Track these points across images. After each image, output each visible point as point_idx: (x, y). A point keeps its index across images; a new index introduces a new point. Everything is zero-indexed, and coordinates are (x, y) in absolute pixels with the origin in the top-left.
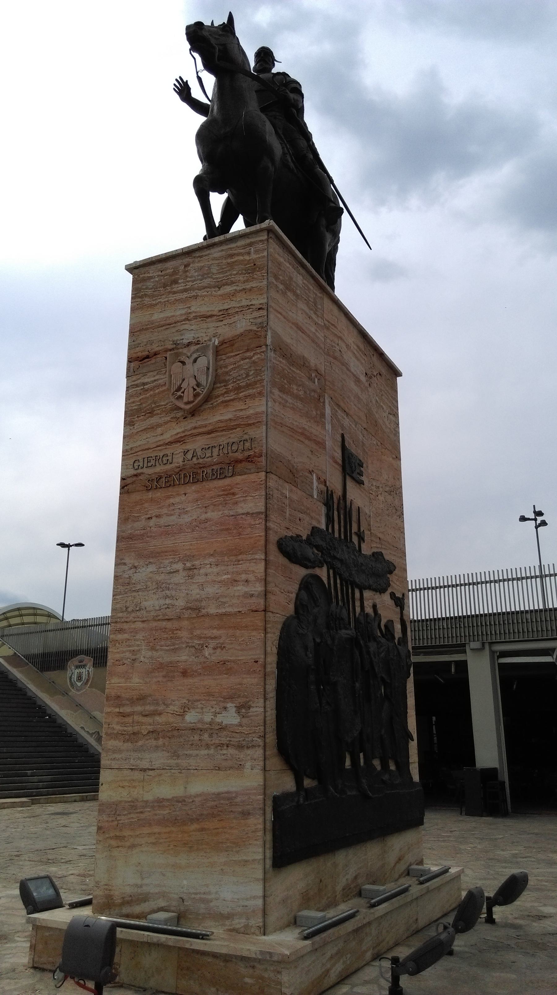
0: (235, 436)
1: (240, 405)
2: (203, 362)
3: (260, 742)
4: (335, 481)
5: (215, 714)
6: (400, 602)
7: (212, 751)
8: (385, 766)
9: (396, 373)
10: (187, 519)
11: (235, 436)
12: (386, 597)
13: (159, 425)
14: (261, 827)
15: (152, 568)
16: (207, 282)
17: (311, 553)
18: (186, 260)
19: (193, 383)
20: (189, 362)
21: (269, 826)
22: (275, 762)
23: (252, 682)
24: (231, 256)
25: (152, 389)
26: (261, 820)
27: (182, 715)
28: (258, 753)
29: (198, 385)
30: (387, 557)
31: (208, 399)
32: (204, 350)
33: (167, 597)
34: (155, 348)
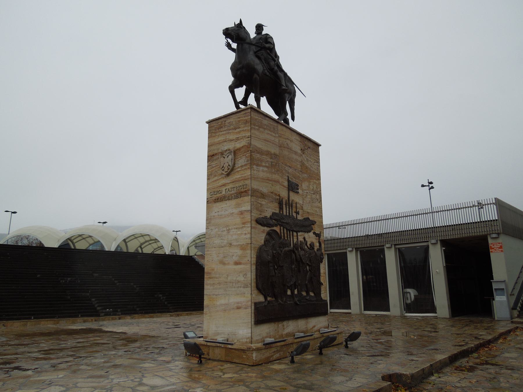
0: (241, 184)
1: (242, 172)
2: (230, 157)
3: (250, 286)
4: (284, 193)
5: (237, 277)
6: (318, 235)
8: (308, 293)
9: (318, 145)
10: (227, 213)
12: (311, 234)
13: (218, 180)
14: (250, 312)
15: (217, 230)
16: (232, 127)
17: (271, 222)
18: (225, 119)
19: (227, 165)
20: (226, 157)
21: (253, 311)
22: (256, 291)
23: (248, 267)
24: (239, 118)
25: (215, 167)
26: (250, 310)
28: (249, 289)
29: (229, 165)
30: (311, 219)
31: (232, 170)
32: (231, 152)
34: (216, 152)
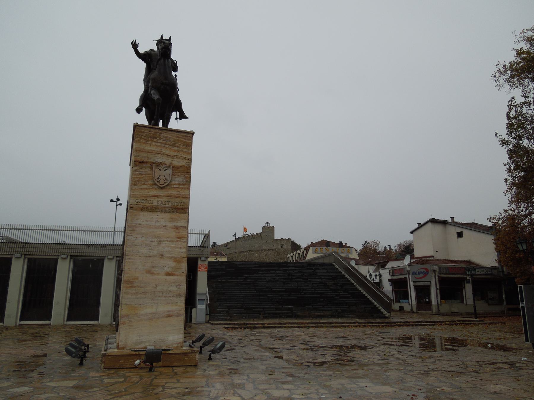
1: (179, 190)
7: (167, 298)
11: (178, 200)
13: (147, 189)
15: (143, 239)
27: (156, 288)
32: (169, 167)
33: (150, 249)
34: (146, 159)
